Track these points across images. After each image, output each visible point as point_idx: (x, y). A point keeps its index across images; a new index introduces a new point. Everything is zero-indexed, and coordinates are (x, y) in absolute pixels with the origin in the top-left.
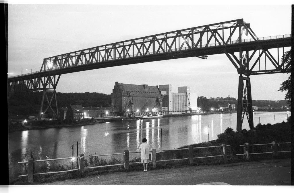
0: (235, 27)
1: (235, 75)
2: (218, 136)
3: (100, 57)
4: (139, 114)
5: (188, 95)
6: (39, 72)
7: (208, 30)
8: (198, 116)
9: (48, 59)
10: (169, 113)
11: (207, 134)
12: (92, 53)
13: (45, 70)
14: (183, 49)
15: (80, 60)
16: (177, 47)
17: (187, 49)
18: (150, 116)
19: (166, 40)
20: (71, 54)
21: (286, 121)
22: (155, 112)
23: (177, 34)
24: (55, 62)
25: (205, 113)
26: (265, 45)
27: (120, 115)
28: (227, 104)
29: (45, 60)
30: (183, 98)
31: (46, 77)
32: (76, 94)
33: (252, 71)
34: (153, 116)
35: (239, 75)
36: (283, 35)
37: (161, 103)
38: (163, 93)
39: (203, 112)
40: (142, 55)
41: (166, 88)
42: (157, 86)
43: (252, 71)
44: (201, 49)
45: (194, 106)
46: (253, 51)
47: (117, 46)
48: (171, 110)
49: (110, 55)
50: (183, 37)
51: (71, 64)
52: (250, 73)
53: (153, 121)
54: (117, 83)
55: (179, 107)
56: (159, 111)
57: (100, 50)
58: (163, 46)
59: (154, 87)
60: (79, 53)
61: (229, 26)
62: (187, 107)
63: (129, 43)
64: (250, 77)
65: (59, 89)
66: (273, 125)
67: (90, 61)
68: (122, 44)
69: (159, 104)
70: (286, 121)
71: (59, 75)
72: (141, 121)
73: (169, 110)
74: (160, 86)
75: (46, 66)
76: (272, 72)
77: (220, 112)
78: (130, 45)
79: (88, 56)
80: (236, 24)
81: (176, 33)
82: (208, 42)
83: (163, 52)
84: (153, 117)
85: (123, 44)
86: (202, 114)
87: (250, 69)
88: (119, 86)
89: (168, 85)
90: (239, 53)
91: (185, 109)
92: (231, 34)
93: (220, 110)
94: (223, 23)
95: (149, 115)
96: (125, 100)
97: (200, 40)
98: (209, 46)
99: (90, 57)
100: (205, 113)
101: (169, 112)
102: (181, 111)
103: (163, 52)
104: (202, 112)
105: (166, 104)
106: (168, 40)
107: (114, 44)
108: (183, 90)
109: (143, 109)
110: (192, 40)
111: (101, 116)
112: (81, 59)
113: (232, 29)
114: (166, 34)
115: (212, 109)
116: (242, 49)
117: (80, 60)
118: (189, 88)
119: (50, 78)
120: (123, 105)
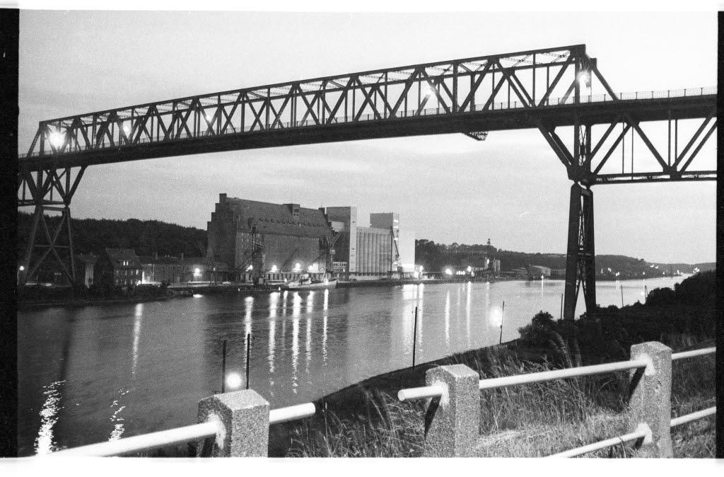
0: (565, 65)
1: (563, 183)
2: (521, 331)
3: (205, 122)
4: (276, 277)
5: (395, 234)
6: (25, 156)
7: (422, 76)
8: (416, 286)
9: (51, 122)
10: (350, 277)
11: (499, 325)
12: (139, 118)
13: (113, 143)
14: (363, 118)
15: (106, 136)
16: (350, 113)
17: (372, 118)
18: (306, 283)
19: (324, 95)
20: (119, 113)
21: (643, 302)
22: (315, 274)
23: (487, 66)
24: (70, 134)
25: (432, 278)
26: (632, 113)
27: (230, 277)
28: (484, 261)
29: (43, 127)
30: (384, 241)
31: (44, 172)
32: (104, 221)
33: (600, 173)
34: (313, 282)
35: (572, 182)
36: (685, 90)
37: (333, 251)
38: (337, 226)
39: (429, 277)
40: (265, 127)
41: (344, 214)
42: (322, 210)
43: (600, 173)
44: (474, 115)
45: (408, 263)
46: (607, 126)
47: (250, 98)
48: (354, 271)
49: (184, 125)
50: (430, 83)
51: (116, 139)
52: (593, 178)
53: (312, 294)
54: (223, 196)
55: (372, 265)
56: (328, 271)
57: (159, 112)
58: (315, 108)
59: (315, 210)
60: (143, 111)
61: (544, 62)
62: (392, 263)
63: (234, 98)
64: (593, 188)
65: (81, 209)
66: (604, 309)
67: (134, 138)
68: (263, 93)
69: (328, 253)
70: (643, 302)
71: (80, 168)
72: (282, 297)
73: (350, 271)
74: (327, 208)
75: (46, 141)
76: (650, 177)
77: (467, 278)
78: (235, 104)
79: (167, 120)
80: (484, 65)
81: (290, 87)
83: (314, 123)
84: (313, 285)
85: (219, 100)
86: (425, 283)
87: (593, 170)
88: (228, 204)
89: (349, 208)
90: (571, 129)
91: (386, 269)
93: (466, 274)
94: (534, 53)
95: (302, 281)
96: (244, 240)
98: (422, 113)
99: (134, 129)
100: (432, 278)
101: (350, 274)
102: (376, 274)
103: (314, 123)
104: (426, 278)
105: (343, 255)
106: (327, 95)
107: (243, 92)
108: (383, 222)
109: (286, 265)
110: (384, 98)
111: (182, 280)
112: (111, 132)
113: (555, 71)
114: (385, 71)
115: (449, 271)
116: (578, 120)
117: (106, 136)
118: (398, 218)
119: (56, 175)
120: (240, 254)
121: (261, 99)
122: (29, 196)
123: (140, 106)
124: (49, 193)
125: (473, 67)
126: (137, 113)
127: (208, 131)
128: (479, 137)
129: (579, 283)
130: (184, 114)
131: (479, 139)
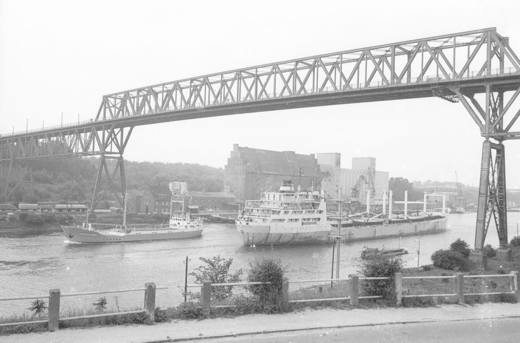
20: (154, 89)
31: (106, 131)
35: (484, 139)
36: (510, 68)
60: (170, 87)
64: (504, 143)
68: (253, 71)
78: (269, 74)
82: (424, 71)
92: (471, 59)
97: (408, 68)
113: (473, 48)
114: (341, 54)
121: (253, 75)
122: (97, 149)
123: (168, 84)
124: (109, 146)
125: (409, 48)
126: (166, 88)
127: (454, 77)
128: (454, 100)
129: (490, 216)
130: (198, 88)
131: (453, 102)
